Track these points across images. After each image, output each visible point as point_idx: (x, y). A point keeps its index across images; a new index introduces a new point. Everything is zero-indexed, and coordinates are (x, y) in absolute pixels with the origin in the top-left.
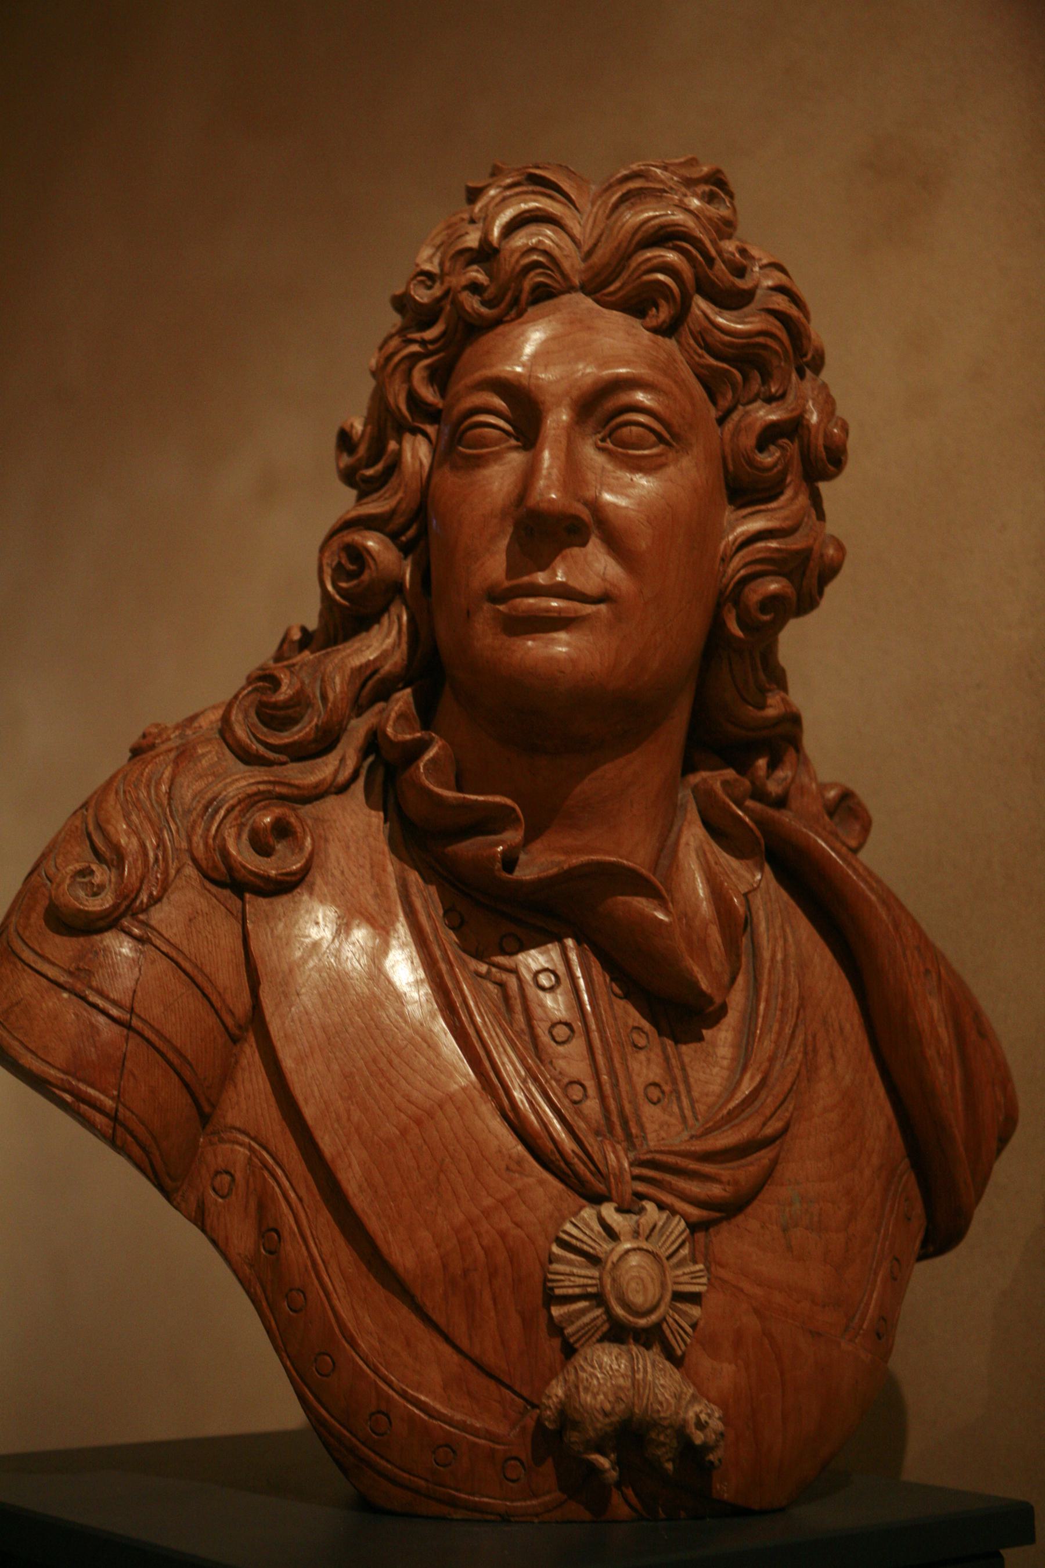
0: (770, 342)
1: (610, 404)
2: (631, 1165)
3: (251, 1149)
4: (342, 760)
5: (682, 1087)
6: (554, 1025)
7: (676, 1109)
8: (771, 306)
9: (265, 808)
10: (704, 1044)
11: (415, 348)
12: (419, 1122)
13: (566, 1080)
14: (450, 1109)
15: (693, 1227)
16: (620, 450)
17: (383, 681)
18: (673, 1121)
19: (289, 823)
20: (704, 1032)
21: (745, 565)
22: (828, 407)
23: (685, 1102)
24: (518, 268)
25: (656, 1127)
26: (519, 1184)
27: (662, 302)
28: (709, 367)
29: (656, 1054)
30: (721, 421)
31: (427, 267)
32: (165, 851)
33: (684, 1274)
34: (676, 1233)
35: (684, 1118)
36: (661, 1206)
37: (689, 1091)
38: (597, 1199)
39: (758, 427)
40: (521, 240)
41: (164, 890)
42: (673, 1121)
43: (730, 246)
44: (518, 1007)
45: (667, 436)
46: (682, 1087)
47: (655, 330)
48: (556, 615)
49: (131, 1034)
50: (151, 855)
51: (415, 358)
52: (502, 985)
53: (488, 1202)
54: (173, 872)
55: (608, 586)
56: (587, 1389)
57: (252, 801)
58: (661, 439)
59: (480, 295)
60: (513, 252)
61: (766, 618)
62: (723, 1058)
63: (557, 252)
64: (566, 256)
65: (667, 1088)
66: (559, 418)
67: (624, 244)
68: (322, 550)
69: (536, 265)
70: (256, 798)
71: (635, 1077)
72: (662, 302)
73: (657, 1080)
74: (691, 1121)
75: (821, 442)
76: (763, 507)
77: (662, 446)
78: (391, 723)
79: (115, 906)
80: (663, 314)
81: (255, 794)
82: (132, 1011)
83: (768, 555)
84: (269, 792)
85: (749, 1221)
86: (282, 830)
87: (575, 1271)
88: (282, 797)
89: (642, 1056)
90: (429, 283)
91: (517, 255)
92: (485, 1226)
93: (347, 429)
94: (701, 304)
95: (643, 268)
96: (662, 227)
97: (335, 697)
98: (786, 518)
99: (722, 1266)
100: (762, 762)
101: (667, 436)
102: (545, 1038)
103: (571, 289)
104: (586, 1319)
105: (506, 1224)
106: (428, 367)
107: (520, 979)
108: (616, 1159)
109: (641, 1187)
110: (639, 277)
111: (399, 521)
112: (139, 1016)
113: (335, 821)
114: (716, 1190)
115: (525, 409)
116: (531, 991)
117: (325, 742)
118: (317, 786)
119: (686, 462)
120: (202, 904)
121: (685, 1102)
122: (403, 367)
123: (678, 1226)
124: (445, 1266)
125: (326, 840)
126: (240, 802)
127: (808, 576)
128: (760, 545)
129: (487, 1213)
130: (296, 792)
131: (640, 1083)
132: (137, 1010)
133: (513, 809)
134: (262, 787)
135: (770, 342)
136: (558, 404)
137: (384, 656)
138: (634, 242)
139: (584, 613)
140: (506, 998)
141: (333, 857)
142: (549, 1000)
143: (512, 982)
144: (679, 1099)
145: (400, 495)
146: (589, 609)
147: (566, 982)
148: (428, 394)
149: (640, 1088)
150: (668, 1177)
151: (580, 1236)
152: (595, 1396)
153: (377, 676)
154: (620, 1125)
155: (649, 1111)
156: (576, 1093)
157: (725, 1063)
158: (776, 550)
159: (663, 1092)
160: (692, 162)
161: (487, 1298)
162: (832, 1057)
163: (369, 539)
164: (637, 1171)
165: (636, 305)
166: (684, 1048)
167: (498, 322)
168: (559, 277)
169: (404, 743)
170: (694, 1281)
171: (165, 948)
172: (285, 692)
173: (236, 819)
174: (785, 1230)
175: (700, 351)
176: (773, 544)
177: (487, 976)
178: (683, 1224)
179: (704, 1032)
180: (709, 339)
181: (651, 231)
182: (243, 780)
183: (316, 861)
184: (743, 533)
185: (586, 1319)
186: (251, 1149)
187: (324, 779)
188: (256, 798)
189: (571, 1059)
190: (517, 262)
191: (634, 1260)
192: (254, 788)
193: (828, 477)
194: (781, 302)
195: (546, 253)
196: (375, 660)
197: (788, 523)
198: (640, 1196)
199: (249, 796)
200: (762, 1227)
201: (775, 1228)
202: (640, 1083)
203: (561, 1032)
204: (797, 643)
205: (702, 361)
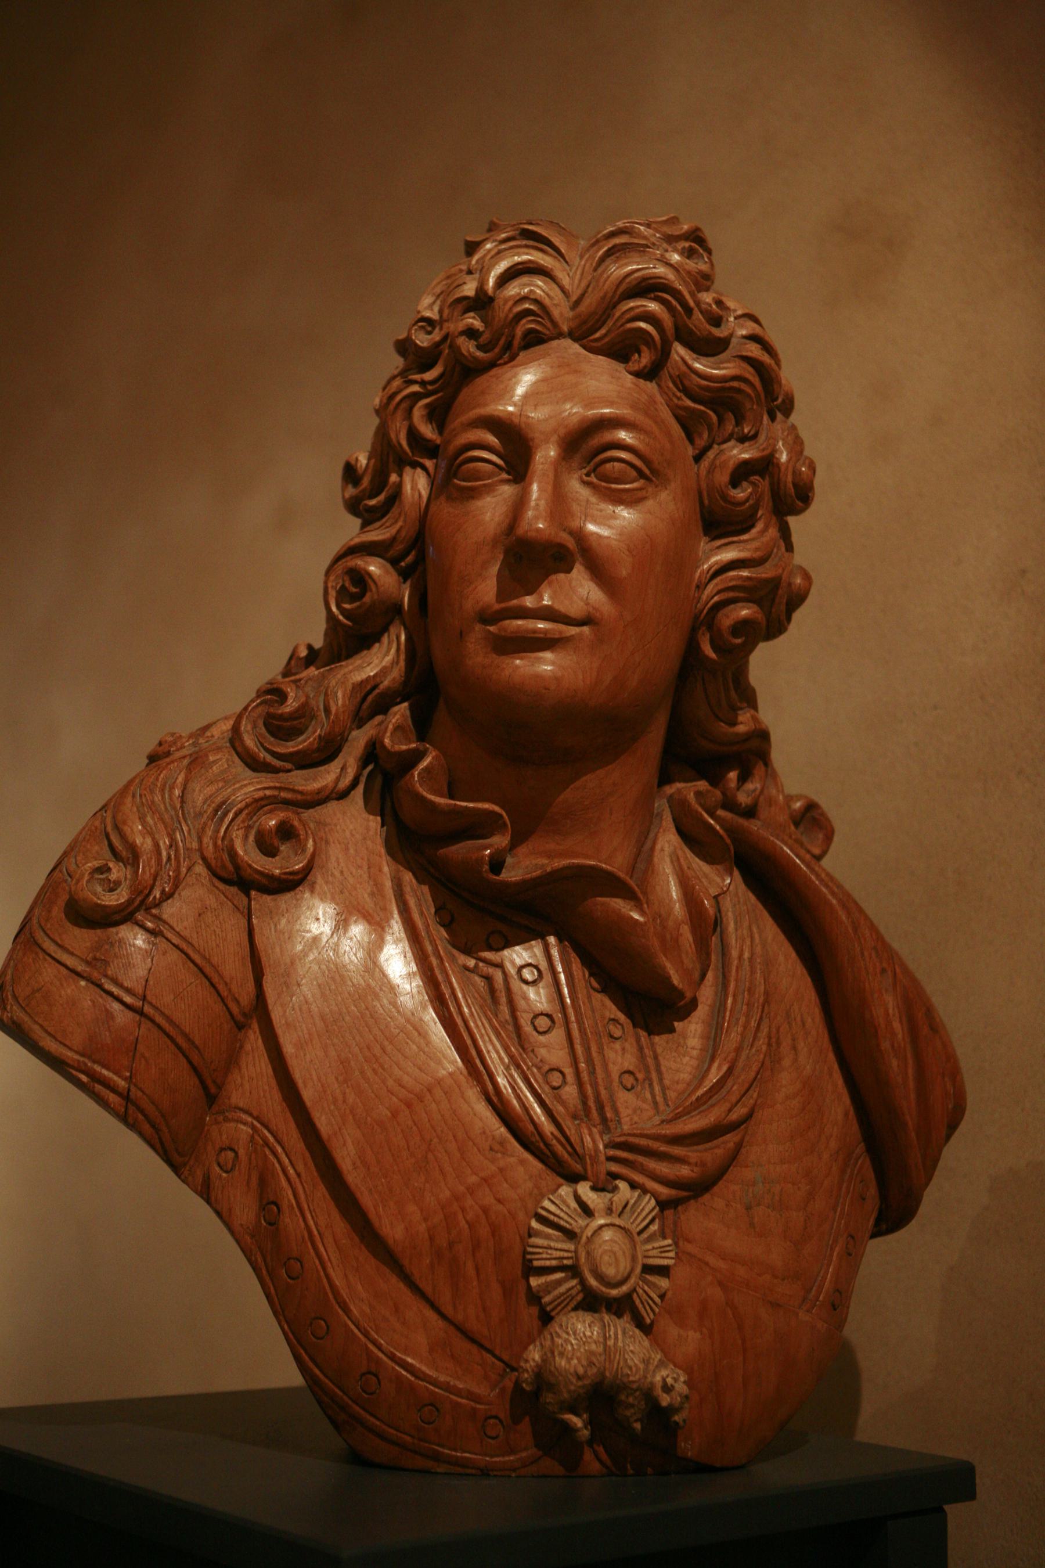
0: (743, 386)
1: (596, 441)
2: (606, 1146)
3: (253, 1127)
4: (343, 768)
5: (654, 1076)
6: (536, 1016)
7: (648, 1096)
8: (744, 354)
9: (271, 811)
10: (675, 1035)
11: (416, 388)
12: (409, 1105)
13: (546, 1068)
14: (438, 1093)
15: (663, 1205)
16: (603, 484)
17: (382, 695)
18: (645, 1106)
19: (292, 826)
20: (676, 1024)
21: (719, 592)
22: (797, 446)
23: (657, 1089)
24: (511, 316)
25: (630, 1111)
26: (502, 1163)
27: (644, 348)
28: (686, 409)
29: (630, 1046)
30: (697, 459)
31: (428, 314)
32: (177, 851)
33: (654, 1248)
34: (644, 1213)
35: (655, 1103)
36: (633, 1186)
37: (661, 1080)
38: (573, 1178)
39: (731, 464)
40: (514, 289)
41: (176, 886)
42: (645, 1106)
43: (707, 298)
44: (503, 1000)
45: (647, 472)
46: (654, 1076)
47: (637, 374)
48: (542, 635)
49: (143, 1019)
50: (164, 854)
51: (416, 397)
52: (488, 979)
53: (473, 1179)
54: (184, 870)
55: (591, 610)
56: (562, 1354)
57: (258, 805)
58: (641, 474)
59: (476, 340)
60: (506, 301)
61: (739, 641)
62: (693, 1048)
63: (547, 301)
64: (556, 305)
65: (640, 1076)
66: (547, 454)
67: (610, 295)
68: (328, 573)
69: (528, 312)
70: (263, 803)
71: (611, 1066)
72: (644, 348)
73: (631, 1068)
74: (662, 1107)
75: (790, 479)
76: (735, 539)
77: (642, 481)
78: (388, 734)
79: (130, 902)
80: (645, 359)
81: (261, 799)
82: (144, 998)
83: (739, 583)
84: (274, 796)
85: (715, 1200)
86: (286, 832)
87: (552, 1244)
88: (287, 802)
89: (617, 1046)
90: (429, 329)
91: (510, 303)
92: (469, 1202)
93: (353, 462)
94: (679, 351)
95: (628, 316)
96: (645, 279)
97: (337, 710)
98: (757, 549)
99: (689, 1242)
100: (733, 775)
101: (647, 472)
102: (528, 1029)
103: (560, 335)
104: (562, 1289)
105: (489, 1200)
106: (427, 406)
107: (505, 974)
108: (592, 1141)
109: (614, 1168)
110: (622, 325)
111: (399, 547)
112: (150, 1003)
113: (336, 825)
114: (685, 1171)
115: (515, 446)
116: (516, 985)
117: (327, 751)
118: (319, 791)
119: (664, 496)
120: (211, 901)
121: (657, 1089)
122: (403, 405)
123: (649, 1204)
124: (431, 1238)
125: (327, 842)
126: (247, 806)
127: (777, 603)
128: (732, 573)
129: (471, 1190)
130: (299, 797)
131: (615, 1071)
132: (149, 998)
133: (501, 816)
134: (268, 793)
135: (743, 386)
136: (547, 441)
137: (384, 672)
138: (618, 293)
139: (568, 634)
140: (492, 991)
141: (333, 859)
142: (531, 993)
143: (498, 976)
144: (651, 1085)
145: (400, 524)
146: (573, 630)
147: (548, 977)
148: (427, 431)
149: (615, 1076)
150: (640, 1159)
151: (558, 1212)
152: (569, 1360)
153: (377, 691)
154: (596, 1109)
155: (623, 1098)
156: (556, 1079)
157: (695, 1053)
158: (748, 578)
159: (637, 1080)
160: (674, 221)
161: (471, 1272)
162: (794, 1048)
163: (370, 564)
164: (611, 1152)
165: (621, 350)
166: (657, 1039)
167: (492, 365)
168: (549, 325)
169: (400, 753)
170: (663, 1255)
171: (176, 940)
172: (291, 705)
173: (243, 822)
174: (748, 1208)
175: (679, 394)
176: (745, 573)
177: (474, 970)
178: (653, 1202)
179: (676, 1024)
180: (687, 383)
181: (634, 283)
182: (250, 786)
183: (317, 862)
184: (716, 563)
185: (562, 1289)
186: (253, 1127)
187: (326, 786)
188: (263, 803)
189: (551, 1048)
190: (511, 309)
191: (607, 1235)
192: (261, 794)
193: (797, 512)
194: (754, 350)
195: (537, 301)
196: (375, 676)
197: (757, 555)
198: (615, 1176)
199: (256, 801)
200: (727, 1205)
201: (739, 1206)
202: (615, 1071)
203: (543, 1023)
204: (764, 663)
205: (680, 403)
